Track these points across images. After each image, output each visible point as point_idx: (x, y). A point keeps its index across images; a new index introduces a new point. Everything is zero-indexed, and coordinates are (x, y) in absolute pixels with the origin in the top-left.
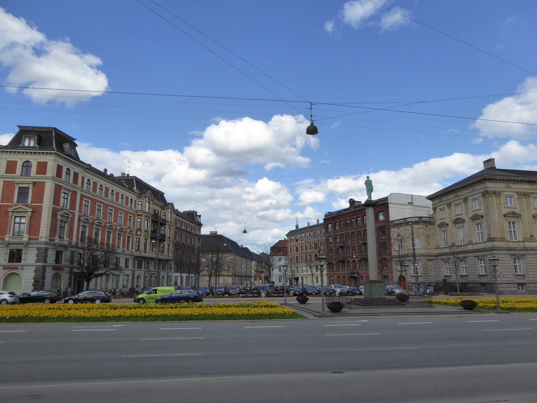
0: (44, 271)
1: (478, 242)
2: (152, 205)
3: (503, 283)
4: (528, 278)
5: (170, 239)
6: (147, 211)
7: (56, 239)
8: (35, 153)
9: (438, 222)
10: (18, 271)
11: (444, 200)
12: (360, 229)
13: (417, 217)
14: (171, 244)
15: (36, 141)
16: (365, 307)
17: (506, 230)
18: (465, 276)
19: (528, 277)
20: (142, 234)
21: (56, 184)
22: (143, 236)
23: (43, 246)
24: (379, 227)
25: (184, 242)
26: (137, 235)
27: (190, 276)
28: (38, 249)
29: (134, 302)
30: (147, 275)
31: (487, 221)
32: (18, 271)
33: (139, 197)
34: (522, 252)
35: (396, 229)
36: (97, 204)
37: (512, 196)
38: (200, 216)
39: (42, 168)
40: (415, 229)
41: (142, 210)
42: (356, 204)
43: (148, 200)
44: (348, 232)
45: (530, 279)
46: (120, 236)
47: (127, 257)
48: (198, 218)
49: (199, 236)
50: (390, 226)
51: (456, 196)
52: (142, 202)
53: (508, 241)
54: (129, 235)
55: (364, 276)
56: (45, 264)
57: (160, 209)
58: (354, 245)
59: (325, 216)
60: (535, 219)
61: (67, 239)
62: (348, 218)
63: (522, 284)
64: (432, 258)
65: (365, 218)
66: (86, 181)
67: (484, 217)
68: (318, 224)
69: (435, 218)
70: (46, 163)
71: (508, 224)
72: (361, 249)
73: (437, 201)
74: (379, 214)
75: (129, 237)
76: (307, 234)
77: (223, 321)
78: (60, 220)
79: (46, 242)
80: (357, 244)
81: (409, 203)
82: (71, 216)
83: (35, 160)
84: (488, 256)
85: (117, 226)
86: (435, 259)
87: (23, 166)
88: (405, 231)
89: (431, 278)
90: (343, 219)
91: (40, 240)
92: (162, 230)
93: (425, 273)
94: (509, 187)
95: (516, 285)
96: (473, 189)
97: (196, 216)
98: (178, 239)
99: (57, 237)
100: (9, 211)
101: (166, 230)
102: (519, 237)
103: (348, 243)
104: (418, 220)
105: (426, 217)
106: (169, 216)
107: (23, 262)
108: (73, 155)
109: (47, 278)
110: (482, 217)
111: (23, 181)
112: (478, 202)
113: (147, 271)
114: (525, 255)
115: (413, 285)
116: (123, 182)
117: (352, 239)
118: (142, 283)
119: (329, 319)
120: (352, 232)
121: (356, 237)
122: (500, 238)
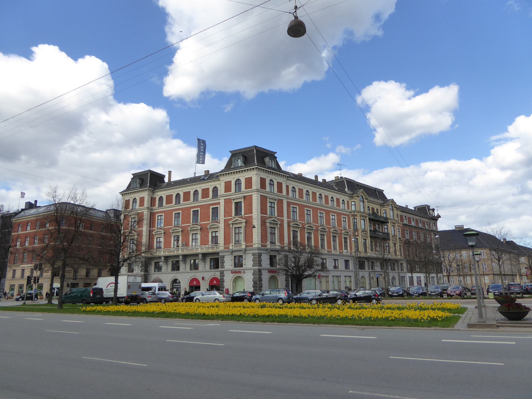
0: (260, 274)
2: (367, 204)
5: (395, 237)
6: (362, 210)
7: (268, 244)
8: (242, 171)
15: (242, 161)
20: (360, 235)
21: (261, 195)
22: (361, 237)
23: (257, 252)
25: (409, 239)
27: (430, 276)
28: (254, 255)
29: (467, 308)
33: (351, 197)
36: (306, 209)
39: (249, 182)
43: (392, 208)
46: (335, 237)
47: (347, 258)
48: (431, 212)
52: (355, 202)
54: (346, 237)
56: (260, 268)
57: (380, 207)
61: (279, 244)
66: (290, 189)
70: (251, 178)
75: (346, 239)
77: (327, 325)
78: (270, 227)
79: (258, 248)
82: (279, 223)
83: (242, 177)
85: (330, 228)
87: (236, 184)
91: (254, 246)
92: (385, 229)
97: (428, 210)
98: (407, 237)
99: (268, 243)
100: (230, 224)
101: (388, 228)
106: (389, 213)
108: (273, 167)
109: (263, 280)
111: (236, 197)
113: (371, 271)
116: (332, 185)
118: (367, 284)
119: (488, 330)
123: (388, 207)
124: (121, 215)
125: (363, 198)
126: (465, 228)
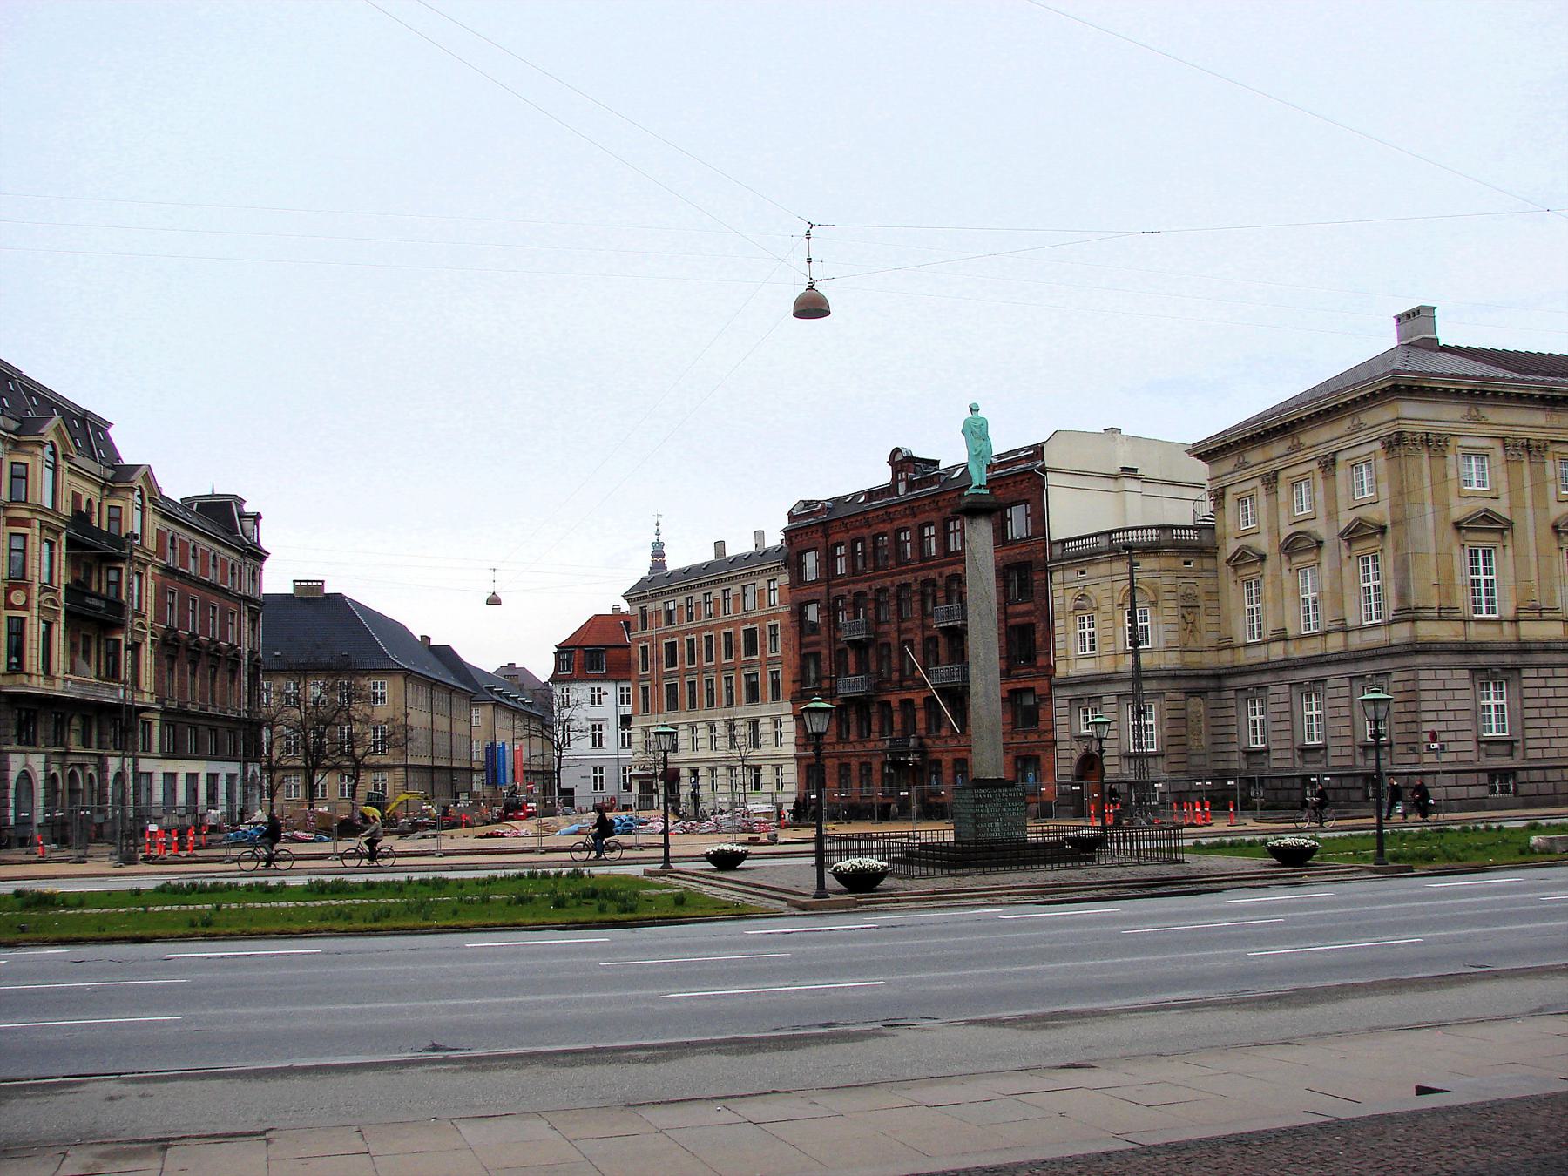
1: (1365, 623)
3: (1437, 772)
4: (1525, 749)
9: (1231, 547)
11: (1252, 463)
12: (933, 574)
13: (1152, 528)
14: (148, 640)
16: (960, 871)
17: (1458, 580)
18: (1316, 749)
19: (1524, 746)
22: (36, 612)
24: (1006, 566)
25: (198, 633)
30: (55, 769)
31: (1396, 547)
34: (1508, 659)
35: (1071, 574)
37: (1485, 452)
38: (257, 518)
40: (1146, 575)
41: (26, 501)
43: (51, 458)
45: (1531, 754)
48: (248, 524)
49: (254, 601)
50: (1052, 561)
51: (1296, 448)
53: (1465, 621)
55: (947, 759)
57: (98, 491)
58: (909, 636)
59: (791, 517)
60: (1559, 539)
62: (882, 528)
63: (1507, 774)
64: (1204, 684)
65: (952, 529)
67: (1389, 529)
69: (1219, 530)
71: (1468, 558)
72: (937, 653)
73: (1227, 465)
74: (1008, 510)
76: (717, 592)
80: (920, 635)
81: (1124, 469)
84: (1395, 677)
86: (1213, 690)
88: (1107, 581)
89: (1196, 760)
90: (865, 532)
93: (1176, 740)
94: (1478, 420)
95: (1484, 778)
96: (1356, 422)
97: (239, 518)
102: (1505, 608)
103: (885, 628)
104: (1155, 538)
105: (1185, 528)
110: (1383, 530)
112: (1369, 474)
114: (1519, 669)
115: (1130, 789)
117: (900, 610)
120: (879, 591)
121: (916, 606)
122: (1440, 609)
123: (39, 451)
125: (54, 453)
126: (328, 590)
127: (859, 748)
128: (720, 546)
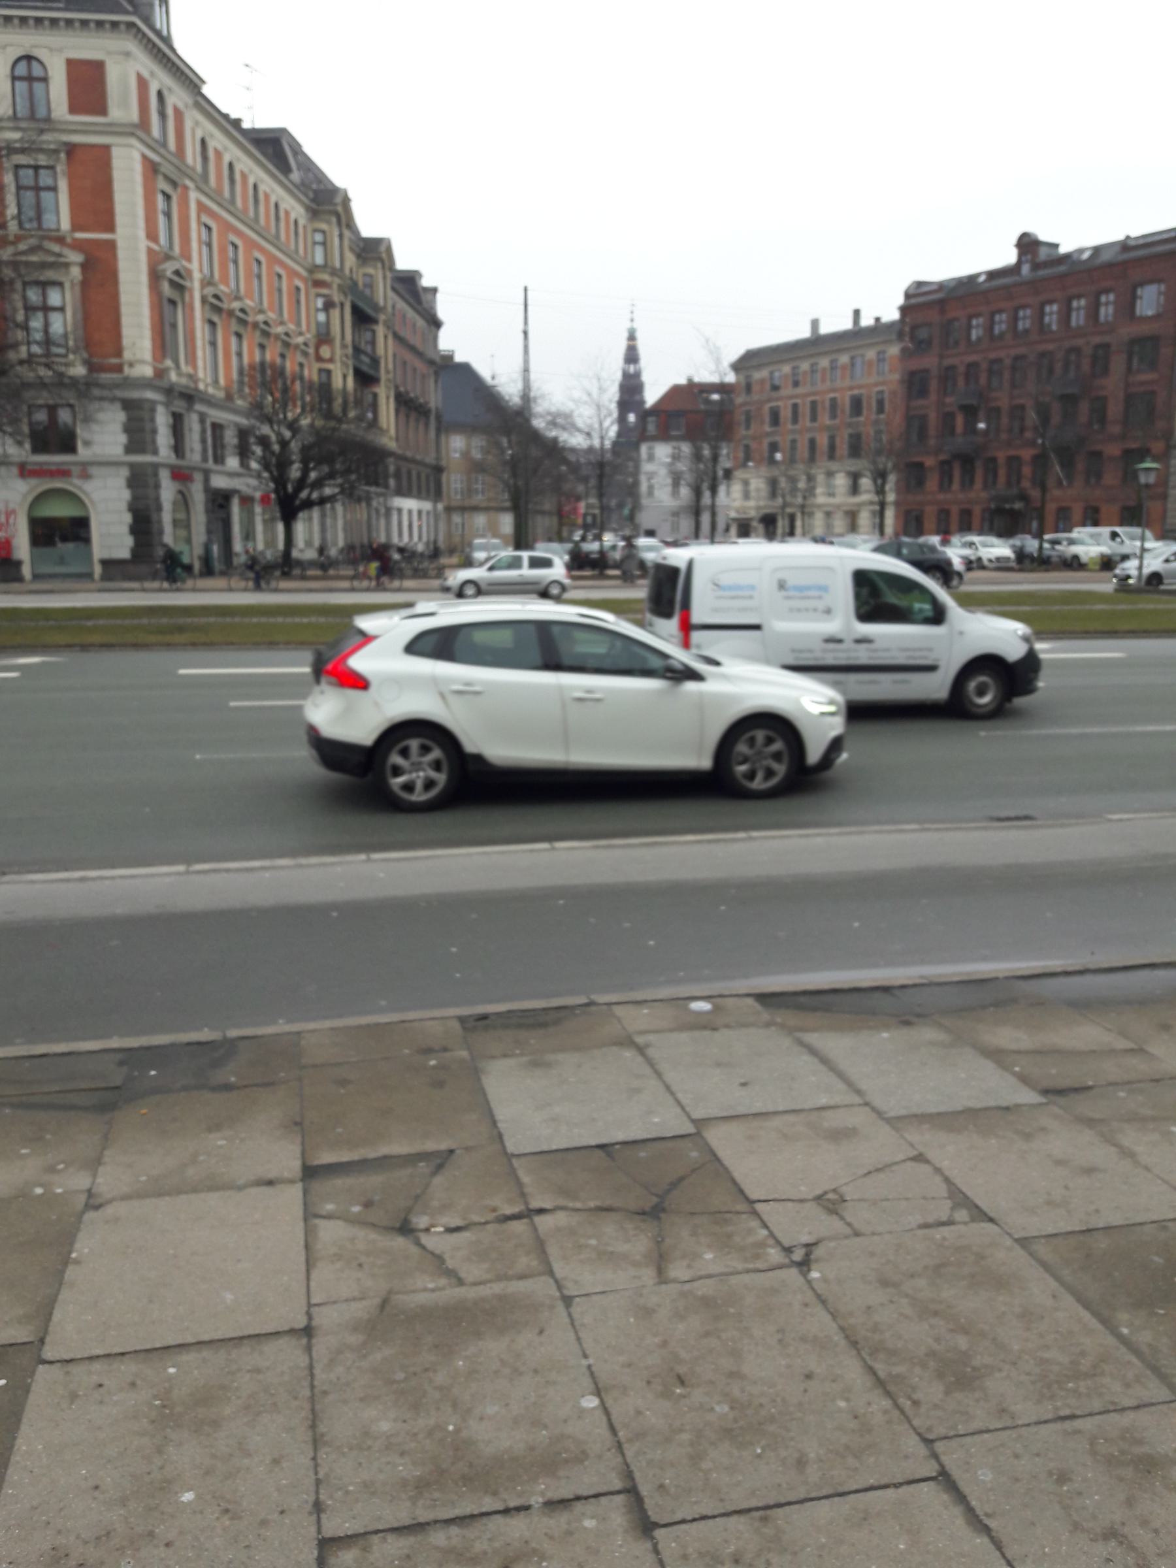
10: (73, 484)
26: (319, 359)
32: (73, 484)
38: (434, 291)
42: (1043, 253)
44: (1002, 354)
59: (908, 295)
68: (857, 328)
76: (824, 362)
107: (83, 453)
120: (1017, 358)
124: (308, 209)
127: (961, 496)
128: (815, 324)
